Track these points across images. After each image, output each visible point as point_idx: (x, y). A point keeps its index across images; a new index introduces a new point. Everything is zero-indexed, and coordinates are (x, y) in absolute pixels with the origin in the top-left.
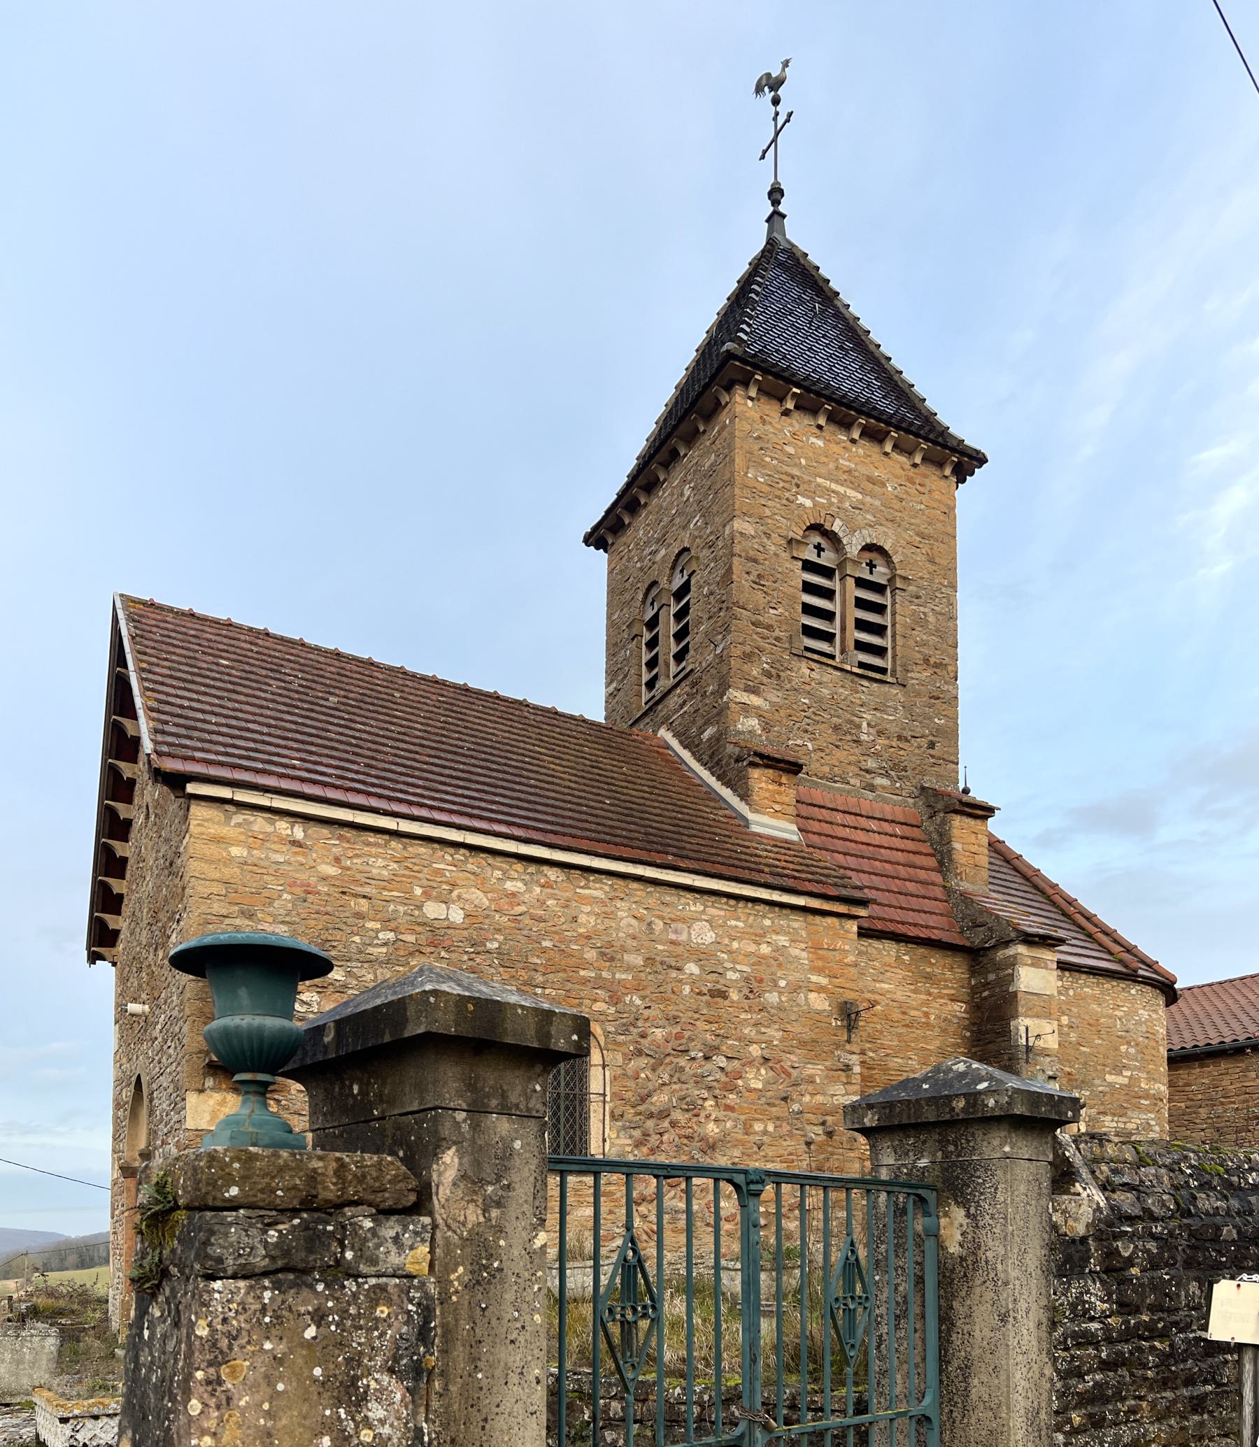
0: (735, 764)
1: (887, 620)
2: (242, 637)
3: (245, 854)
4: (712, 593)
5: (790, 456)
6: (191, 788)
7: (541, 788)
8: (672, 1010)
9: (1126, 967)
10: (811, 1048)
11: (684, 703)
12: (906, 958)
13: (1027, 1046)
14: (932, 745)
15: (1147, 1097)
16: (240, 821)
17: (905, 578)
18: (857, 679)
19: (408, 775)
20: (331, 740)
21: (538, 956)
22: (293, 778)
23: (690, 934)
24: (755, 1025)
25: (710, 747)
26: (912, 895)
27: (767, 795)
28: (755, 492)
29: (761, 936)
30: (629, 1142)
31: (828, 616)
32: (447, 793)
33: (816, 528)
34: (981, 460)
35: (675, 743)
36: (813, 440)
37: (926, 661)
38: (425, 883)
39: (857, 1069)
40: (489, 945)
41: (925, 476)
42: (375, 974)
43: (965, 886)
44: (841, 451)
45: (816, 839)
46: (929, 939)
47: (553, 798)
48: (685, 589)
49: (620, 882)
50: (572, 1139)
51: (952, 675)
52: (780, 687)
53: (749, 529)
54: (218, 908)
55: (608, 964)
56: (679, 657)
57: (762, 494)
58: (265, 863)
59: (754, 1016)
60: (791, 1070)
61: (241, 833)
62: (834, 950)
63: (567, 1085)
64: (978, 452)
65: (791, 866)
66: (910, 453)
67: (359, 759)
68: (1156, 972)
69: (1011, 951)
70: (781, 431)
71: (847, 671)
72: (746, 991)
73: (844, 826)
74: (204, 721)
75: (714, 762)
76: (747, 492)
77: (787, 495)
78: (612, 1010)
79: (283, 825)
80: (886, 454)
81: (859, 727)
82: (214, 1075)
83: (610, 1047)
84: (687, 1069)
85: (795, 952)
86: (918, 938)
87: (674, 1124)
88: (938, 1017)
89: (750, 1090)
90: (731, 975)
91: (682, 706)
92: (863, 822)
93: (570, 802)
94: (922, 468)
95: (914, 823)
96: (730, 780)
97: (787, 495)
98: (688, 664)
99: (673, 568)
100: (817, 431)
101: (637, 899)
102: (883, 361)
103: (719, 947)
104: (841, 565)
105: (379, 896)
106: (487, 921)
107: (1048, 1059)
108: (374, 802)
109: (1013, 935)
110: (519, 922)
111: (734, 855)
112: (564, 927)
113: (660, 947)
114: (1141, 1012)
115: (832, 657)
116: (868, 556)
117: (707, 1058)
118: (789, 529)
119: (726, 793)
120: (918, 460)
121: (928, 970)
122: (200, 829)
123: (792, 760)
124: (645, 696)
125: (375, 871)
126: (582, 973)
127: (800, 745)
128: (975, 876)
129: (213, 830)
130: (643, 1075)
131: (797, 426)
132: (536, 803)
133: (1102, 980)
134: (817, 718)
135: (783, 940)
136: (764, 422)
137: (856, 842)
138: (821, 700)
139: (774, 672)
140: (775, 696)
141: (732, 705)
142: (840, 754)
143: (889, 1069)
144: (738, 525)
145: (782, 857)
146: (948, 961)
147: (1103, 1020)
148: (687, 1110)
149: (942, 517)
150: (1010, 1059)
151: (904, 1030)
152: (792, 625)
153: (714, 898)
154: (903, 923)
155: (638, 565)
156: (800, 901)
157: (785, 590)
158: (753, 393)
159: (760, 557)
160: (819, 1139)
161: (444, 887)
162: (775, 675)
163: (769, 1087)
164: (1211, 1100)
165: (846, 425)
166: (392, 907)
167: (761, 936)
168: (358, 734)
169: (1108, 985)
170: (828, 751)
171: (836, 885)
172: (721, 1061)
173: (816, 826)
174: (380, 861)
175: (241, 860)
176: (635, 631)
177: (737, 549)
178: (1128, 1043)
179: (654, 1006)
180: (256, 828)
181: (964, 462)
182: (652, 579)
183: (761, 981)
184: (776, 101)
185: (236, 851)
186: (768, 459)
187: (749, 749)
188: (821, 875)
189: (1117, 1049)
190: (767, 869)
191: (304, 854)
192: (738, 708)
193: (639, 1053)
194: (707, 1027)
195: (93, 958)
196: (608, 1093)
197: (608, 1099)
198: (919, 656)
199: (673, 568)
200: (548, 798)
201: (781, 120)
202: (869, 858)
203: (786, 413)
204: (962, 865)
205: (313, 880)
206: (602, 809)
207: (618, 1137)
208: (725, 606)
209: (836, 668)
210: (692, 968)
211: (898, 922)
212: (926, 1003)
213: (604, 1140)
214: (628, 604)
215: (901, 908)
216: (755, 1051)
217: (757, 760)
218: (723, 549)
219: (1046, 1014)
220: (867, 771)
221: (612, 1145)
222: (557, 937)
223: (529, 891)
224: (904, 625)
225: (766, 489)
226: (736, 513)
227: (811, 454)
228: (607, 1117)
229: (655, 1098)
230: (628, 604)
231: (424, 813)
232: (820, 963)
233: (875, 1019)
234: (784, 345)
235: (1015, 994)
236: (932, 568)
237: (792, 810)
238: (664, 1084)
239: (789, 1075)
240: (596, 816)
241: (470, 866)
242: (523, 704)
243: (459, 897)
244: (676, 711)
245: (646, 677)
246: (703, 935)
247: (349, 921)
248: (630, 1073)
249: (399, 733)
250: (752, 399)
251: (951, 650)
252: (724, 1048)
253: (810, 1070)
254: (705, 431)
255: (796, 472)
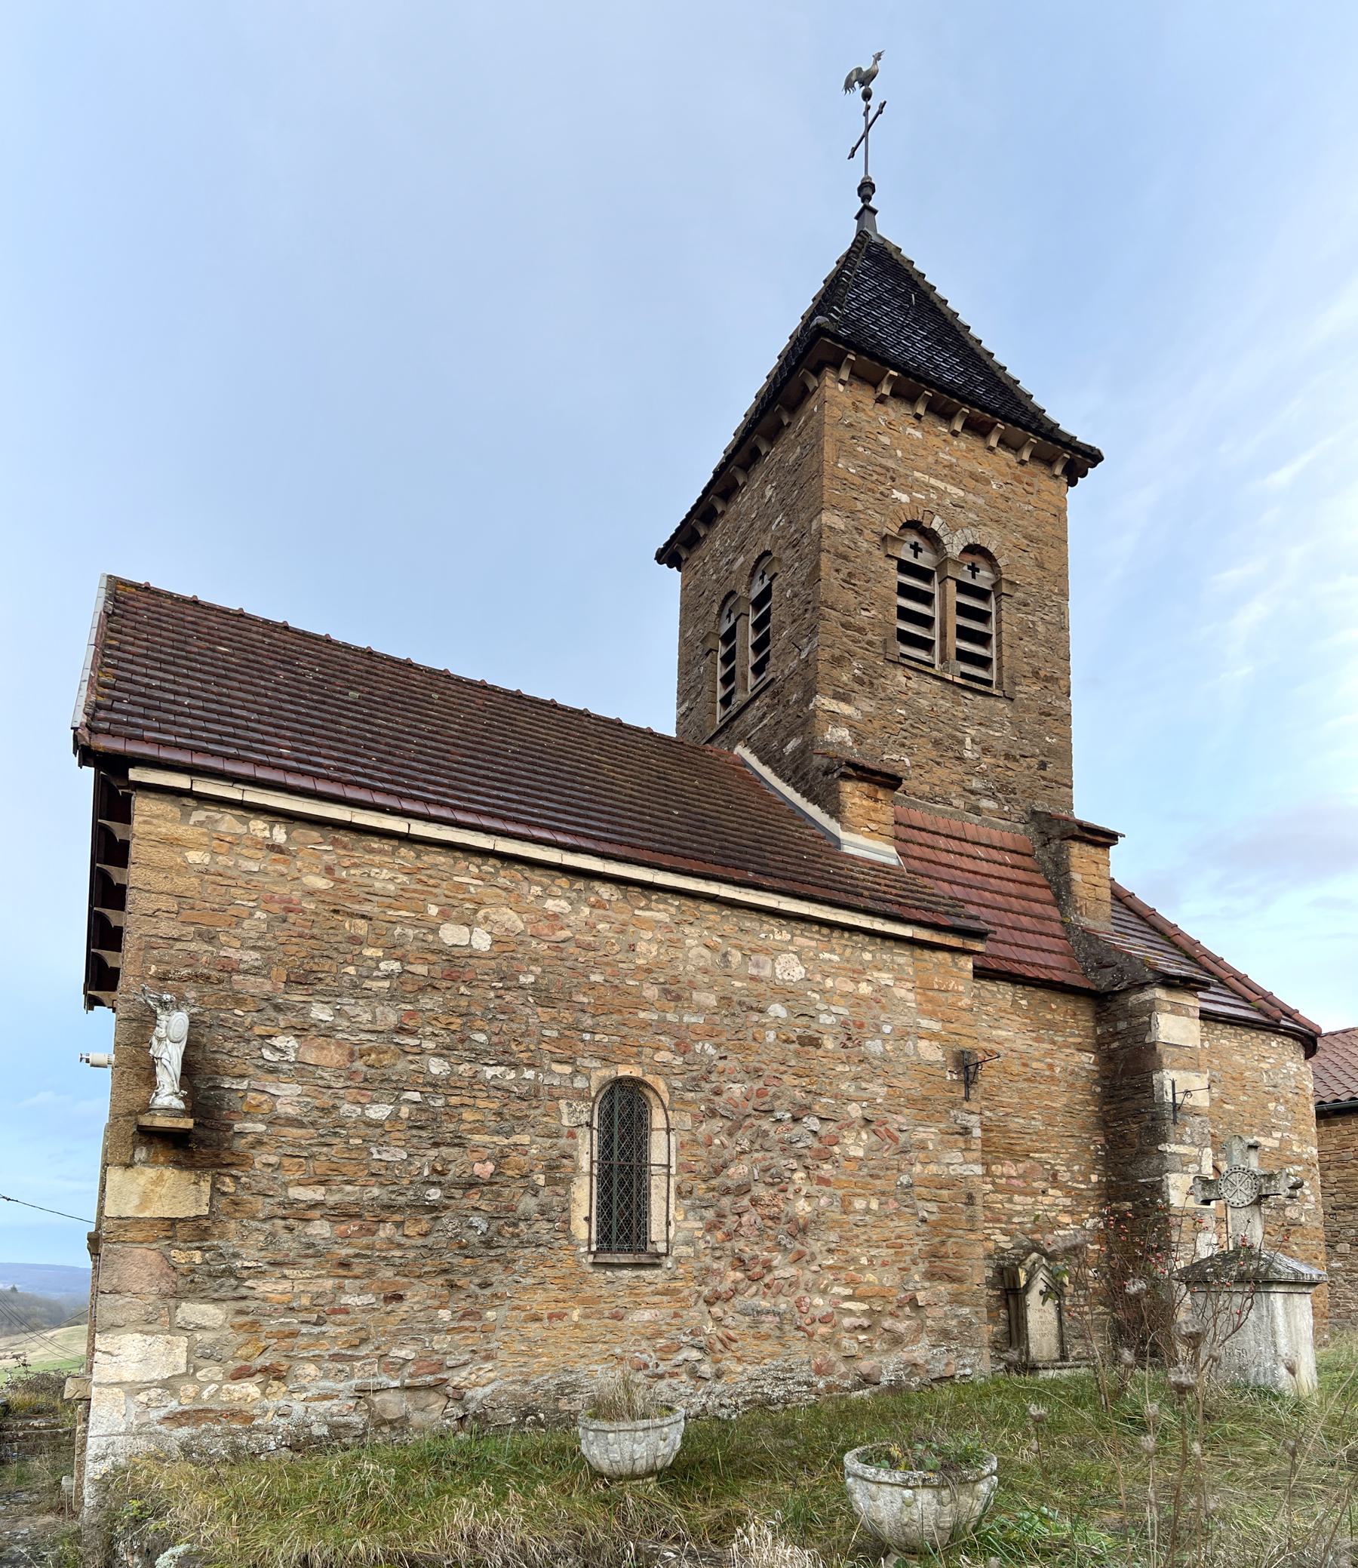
0: (823, 778)
1: (991, 629)
2: (255, 629)
3: (207, 860)
4: (795, 595)
5: (885, 447)
6: (135, 774)
7: (596, 795)
8: (753, 1061)
9: (1267, 1016)
10: (923, 1106)
11: (764, 716)
12: (1024, 1002)
13: (1174, 1104)
14: (1043, 766)
15: (1300, 1162)
16: (202, 818)
17: (1012, 583)
18: (959, 691)
19: (432, 773)
20: (340, 732)
21: (585, 994)
22: (274, 767)
23: (774, 969)
24: (855, 1079)
25: (794, 760)
26: (1028, 931)
27: (861, 812)
28: (845, 483)
29: (860, 972)
30: (700, 1225)
31: (926, 622)
32: (478, 793)
33: (912, 525)
34: (1094, 457)
35: (753, 760)
36: (909, 430)
37: (1036, 674)
38: (444, 900)
39: (977, 1132)
40: (522, 979)
41: (1034, 476)
42: (374, 1013)
43: (1086, 922)
44: (942, 445)
45: (916, 864)
46: (1050, 981)
47: (611, 806)
48: (766, 595)
49: (690, 903)
50: (628, 1222)
51: (1064, 690)
52: (873, 696)
53: (839, 524)
54: (166, 928)
55: (673, 1004)
56: (758, 669)
57: (853, 487)
58: (234, 873)
59: (853, 1068)
60: (898, 1134)
61: (203, 834)
62: (946, 991)
63: (622, 1153)
64: (1092, 449)
65: (894, 891)
66: (1017, 449)
67: (370, 753)
68: (1296, 1022)
69: (1147, 995)
70: (875, 419)
71: (948, 681)
72: (843, 1038)
73: (948, 851)
74: (174, 702)
75: (797, 774)
76: (836, 484)
77: (882, 488)
78: (679, 1061)
79: (258, 826)
80: (991, 449)
81: (962, 742)
82: (148, 1144)
83: (676, 1106)
84: (772, 1133)
85: (901, 993)
86: (1038, 979)
87: (755, 1202)
88: (1064, 1070)
89: (849, 1159)
90: (825, 1019)
91: (761, 719)
92: (969, 848)
93: (630, 810)
94: (1030, 466)
95: (1025, 851)
96: (817, 796)
97: (882, 488)
98: (768, 675)
99: (752, 575)
100: (914, 421)
101: (710, 924)
102: (985, 357)
103: (809, 985)
104: (941, 566)
105: (382, 917)
106: (521, 949)
107: (1198, 1119)
108: (379, 799)
109: (1150, 976)
110: (562, 950)
111: (826, 875)
112: (619, 957)
113: (738, 984)
114: (1289, 1064)
115: (933, 666)
116: (969, 559)
117: (796, 1120)
118: (883, 524)
119: (813, 810)
120: (1026, 456)
121: (1049, 1016)
122: (147, 828)
123: (890, 771)
124: (720, 713)
125: (377, 885)
126: (642, 1015)
127: (894, 758)
128: (1096, 911)
129: (164, 829)
130: (717, 1141)
131: (893, 415)
132: (589, 809)
133: (1240, 1031)
134: (915, 731)
135: (886, 978)
136: (856, 409)
137: (962, 870)
138: (919, 712)
139: (866, 678)
140: (868, 706)
141: (819, 713)
142: (940, 772)
143: (1009, 1131)
144: (826, 518)
145: (883, 882)
146: (1071, 1006)
147: (1247, 1074)
148: (772, 1185)
149: (1051, 520)
150: (1153, 1119)
151: (1025, 1085)
152: (886, 629)
153: (803, 926)
154: (1019, 962)
155: (714, 577)
156: (907, 931)
157: (878, 590)
158: (845, 375)
159: (852, 554)
160: (933, 1218)
161: (467, 905)
162: (867, 682)
163: (872, 1155)
164: (1342, 1161)
165: (947, 417)
166: (399, 930)
167: (860, 972)
168: (376, 729)
169: (1247, 1036)
170: (927, 768)
171: (947, 913)
172: (813, 1124)
173: (917, 851)
174: (384, 872)
175: (200, 868)
176: (709, 646)
177: (825, 543)
178: (1277, 1100)
179: (731, 1056)
180: (223, 827)
181: (1078, 460)
182: (729, 589)
183: (861, 1026)
184: (867, 96)
185: (194, 856)
186: (860, 449)
187: (841, 759)
188: (929, 902)
189: (1265, 1107)
190: (866, 893)
191: (285, 862)
192: (826, 716)
193: (713, 1113)
194: (796, 1082)
195: (92, 1002)
196: (673, 1163)
197: (673, 1171)
198: (1027, 668)
199: (752, 575)
200: (605, 804)
201: (871, 114)
202: (977, 888)
203: (881, 400)
204: (1082, 898)
205: (296, 895)
206: (668, 819)
207: (686, 1219)
208: (811, 609)
209: (935, 677)
210: (777, 1010)
211: (1014, 961)
212: (1049, 1053)
213: (668, 1224)
214: (702, 619)
215: (1017, 945)
216: (855, 1110)
217: (850, 771)
218: (809, 546)
219: (1196, 1067)
220: (972, 792)
221: (678, 1229)
222: (609, 970)
223: (576, 911)
224: (1011, 634)
225: (858, 481)
226: (825, 505)
227: (908, 446)
228: (672, 1195)
229: (732, 1170)
230: (702, 619)
231: (444, 813)
232: (930, 1007)
233: (992, 1072)
234: (881, 328)
235: (1153, 1046)
236: (1040, 573)
237: (889, 830)
238: (743, 1152)
239: (896, 1140)
240: (662, 826)
241: (501, 880)
242: (585, 714)
243: (486, 918)
244: (755, 725)
245: (721, 694)
246: (790, 970)
247: (342, 947)
248: (701, 1138)
249: (430, 732)
250: (843, 383)
251: (1062, 663)
252: (817, 1107)
253: (921, 1134)
254: (789, 424)
255: (890, 464)
